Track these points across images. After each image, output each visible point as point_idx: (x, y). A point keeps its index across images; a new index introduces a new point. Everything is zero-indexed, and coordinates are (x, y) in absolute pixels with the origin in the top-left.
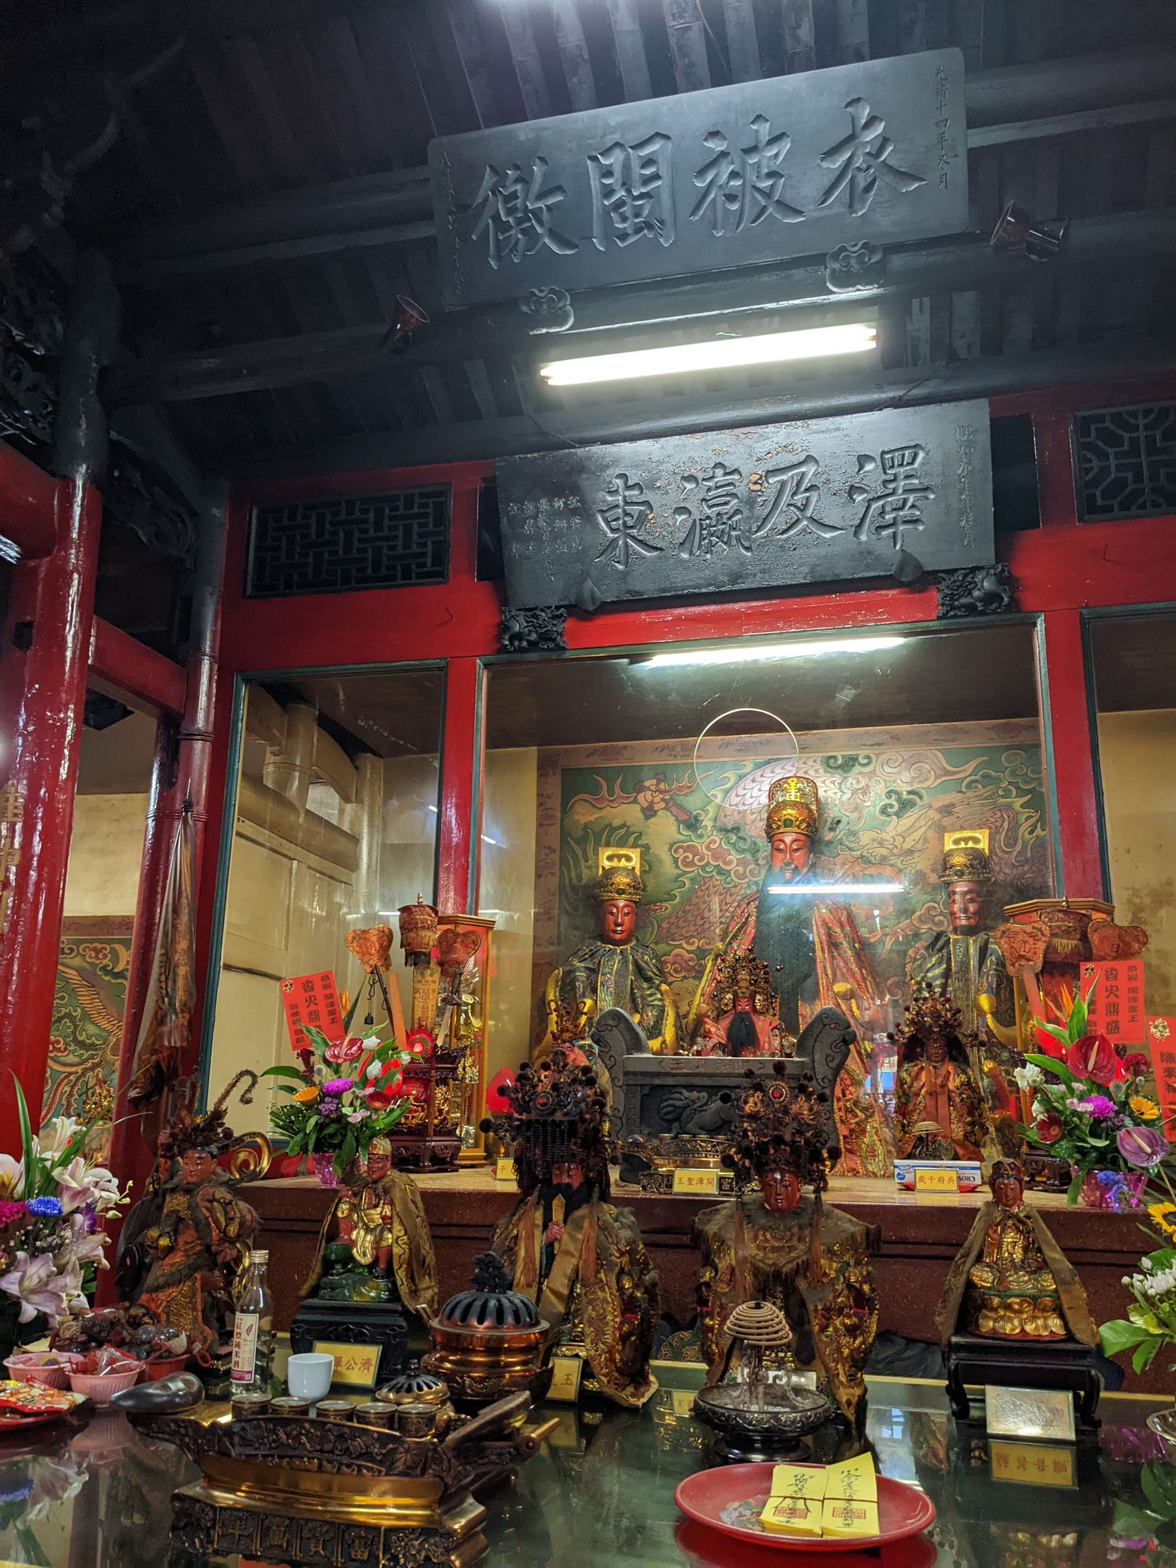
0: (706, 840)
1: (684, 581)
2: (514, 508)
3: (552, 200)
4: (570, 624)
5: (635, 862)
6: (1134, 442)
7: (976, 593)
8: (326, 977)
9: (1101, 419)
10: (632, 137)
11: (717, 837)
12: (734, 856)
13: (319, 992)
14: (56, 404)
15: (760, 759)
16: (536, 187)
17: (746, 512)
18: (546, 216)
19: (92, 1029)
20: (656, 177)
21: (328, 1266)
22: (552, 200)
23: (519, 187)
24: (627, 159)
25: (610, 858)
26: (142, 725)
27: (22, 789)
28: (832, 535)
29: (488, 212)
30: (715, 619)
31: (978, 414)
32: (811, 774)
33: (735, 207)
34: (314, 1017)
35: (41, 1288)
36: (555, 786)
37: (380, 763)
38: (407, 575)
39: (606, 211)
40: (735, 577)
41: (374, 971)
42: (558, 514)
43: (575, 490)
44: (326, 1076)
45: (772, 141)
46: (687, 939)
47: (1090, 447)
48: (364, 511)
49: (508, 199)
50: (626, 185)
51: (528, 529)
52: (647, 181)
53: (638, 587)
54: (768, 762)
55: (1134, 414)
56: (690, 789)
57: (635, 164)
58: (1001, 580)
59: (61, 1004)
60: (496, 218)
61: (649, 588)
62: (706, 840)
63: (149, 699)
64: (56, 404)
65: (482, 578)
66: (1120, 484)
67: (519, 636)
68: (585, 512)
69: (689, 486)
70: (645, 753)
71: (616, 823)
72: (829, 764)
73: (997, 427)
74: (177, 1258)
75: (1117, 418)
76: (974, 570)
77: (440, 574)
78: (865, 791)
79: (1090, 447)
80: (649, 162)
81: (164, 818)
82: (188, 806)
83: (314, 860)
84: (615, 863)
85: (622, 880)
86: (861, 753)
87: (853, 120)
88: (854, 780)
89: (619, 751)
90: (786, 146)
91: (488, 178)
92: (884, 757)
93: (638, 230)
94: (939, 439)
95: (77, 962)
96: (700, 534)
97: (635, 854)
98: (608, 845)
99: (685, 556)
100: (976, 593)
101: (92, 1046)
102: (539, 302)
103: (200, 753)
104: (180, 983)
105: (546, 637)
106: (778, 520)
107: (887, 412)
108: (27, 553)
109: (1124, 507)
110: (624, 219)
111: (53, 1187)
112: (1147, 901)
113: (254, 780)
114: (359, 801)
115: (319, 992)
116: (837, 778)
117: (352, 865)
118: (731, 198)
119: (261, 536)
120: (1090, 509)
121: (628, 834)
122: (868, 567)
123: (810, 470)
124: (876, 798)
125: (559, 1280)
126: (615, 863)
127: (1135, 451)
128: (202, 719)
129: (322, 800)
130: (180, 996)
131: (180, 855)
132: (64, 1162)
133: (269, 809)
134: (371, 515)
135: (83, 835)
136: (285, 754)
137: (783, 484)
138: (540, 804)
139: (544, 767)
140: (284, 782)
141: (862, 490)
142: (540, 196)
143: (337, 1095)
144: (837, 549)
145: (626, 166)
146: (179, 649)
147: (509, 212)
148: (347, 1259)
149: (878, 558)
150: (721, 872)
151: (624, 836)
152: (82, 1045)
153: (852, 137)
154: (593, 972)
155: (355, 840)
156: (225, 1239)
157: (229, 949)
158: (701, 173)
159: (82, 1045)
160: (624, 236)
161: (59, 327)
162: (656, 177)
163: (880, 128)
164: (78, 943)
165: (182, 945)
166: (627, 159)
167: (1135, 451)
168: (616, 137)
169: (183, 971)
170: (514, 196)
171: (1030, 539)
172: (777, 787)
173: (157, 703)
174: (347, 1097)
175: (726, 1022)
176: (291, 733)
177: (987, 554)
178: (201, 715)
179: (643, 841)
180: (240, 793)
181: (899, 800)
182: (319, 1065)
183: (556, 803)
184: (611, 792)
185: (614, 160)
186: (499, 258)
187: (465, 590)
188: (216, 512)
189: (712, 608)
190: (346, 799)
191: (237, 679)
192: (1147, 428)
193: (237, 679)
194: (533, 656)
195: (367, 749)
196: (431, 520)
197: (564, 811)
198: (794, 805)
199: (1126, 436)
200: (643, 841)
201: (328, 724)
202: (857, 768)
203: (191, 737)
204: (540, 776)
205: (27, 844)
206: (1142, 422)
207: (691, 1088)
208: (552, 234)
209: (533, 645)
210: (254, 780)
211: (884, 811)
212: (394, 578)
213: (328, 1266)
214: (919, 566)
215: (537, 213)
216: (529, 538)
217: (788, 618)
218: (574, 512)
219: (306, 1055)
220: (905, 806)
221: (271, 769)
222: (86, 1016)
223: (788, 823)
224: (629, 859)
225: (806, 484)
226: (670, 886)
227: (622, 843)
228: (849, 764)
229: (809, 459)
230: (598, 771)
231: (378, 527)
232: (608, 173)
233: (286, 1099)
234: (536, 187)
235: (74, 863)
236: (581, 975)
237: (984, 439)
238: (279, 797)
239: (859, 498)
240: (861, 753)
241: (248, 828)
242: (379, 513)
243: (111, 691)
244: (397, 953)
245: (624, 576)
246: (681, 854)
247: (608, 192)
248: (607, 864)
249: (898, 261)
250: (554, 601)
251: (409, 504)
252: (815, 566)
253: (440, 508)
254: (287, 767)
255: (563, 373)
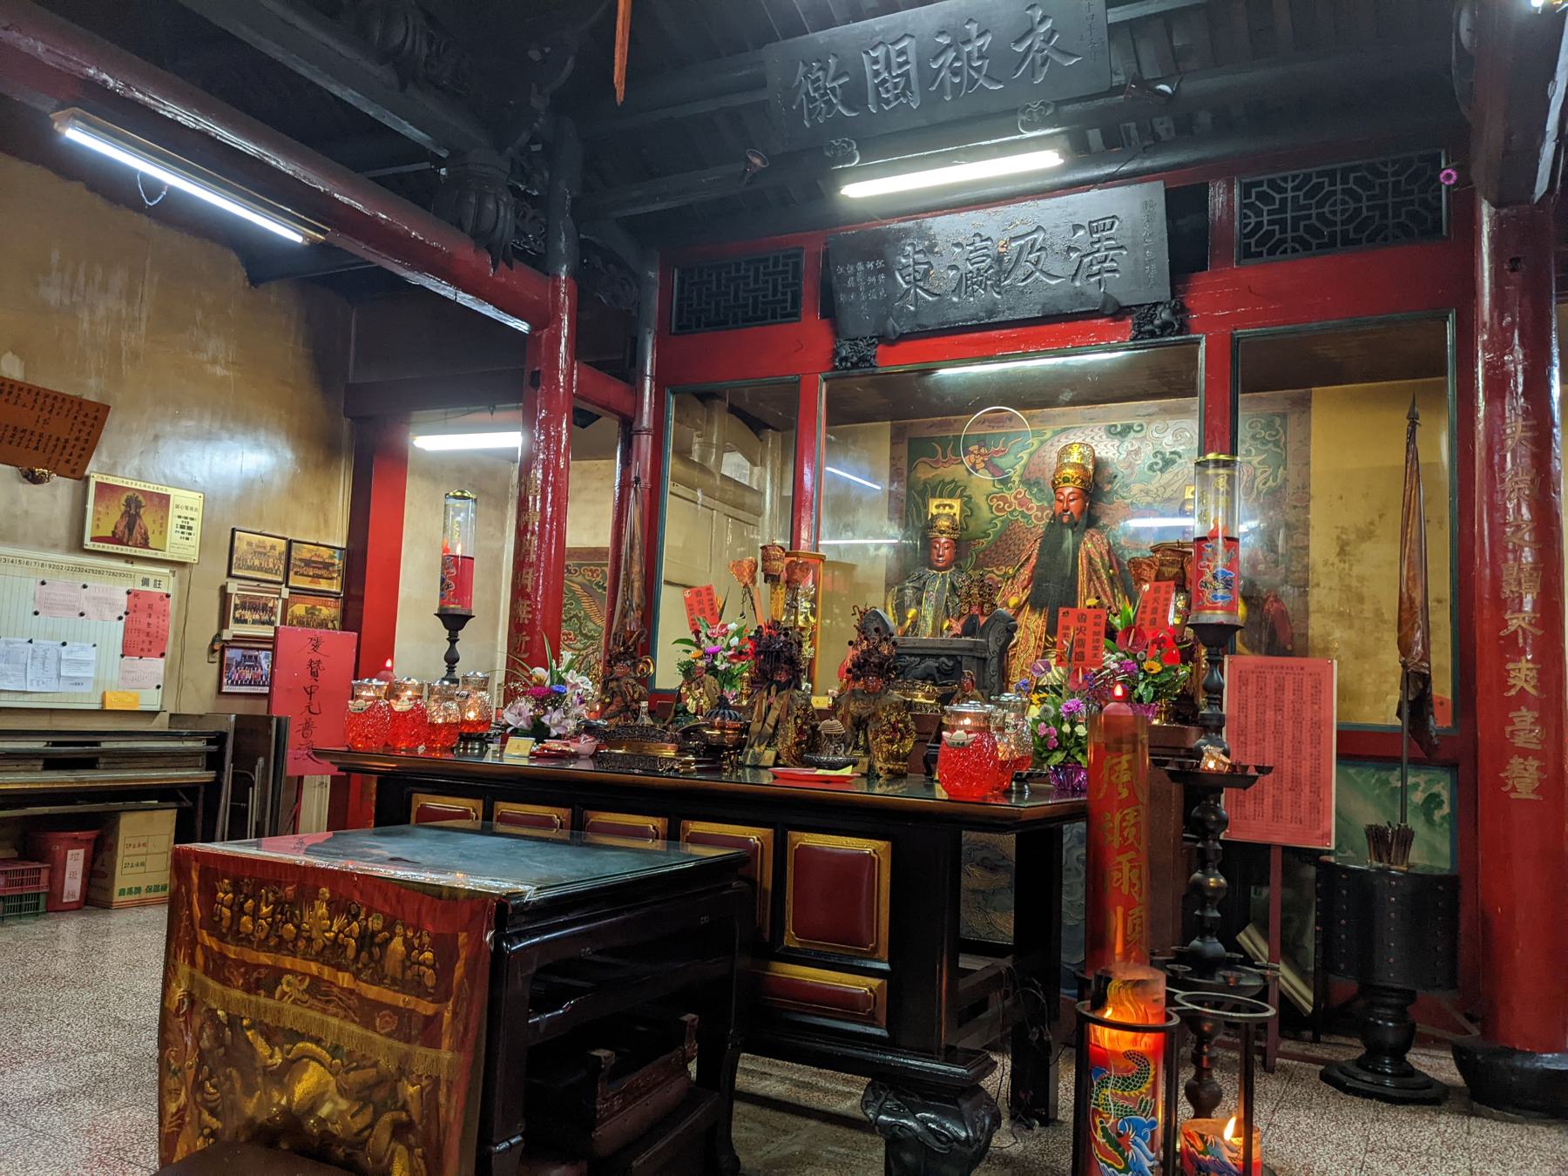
0: (1014, 492)
1: (954, 317)
2: (840, 270)
3: (841, 81)
4: (880, 348)
5: (957, 510)
6: (1283, 201)
7: (1157, 322)
8: (709, 589)
9: (1260, 184)
10: (892, 37)
11: (1022, 489)
12: (1035, 504)
13: (705, 597)
14: (547, 226)
15: (1058, 428)
16: (832, 71)
17: (996, 267)
18: (838, 91)
19: (591, 626)
20: (906, 62)
21: (677, 713)
22: (841, 81)
23: (820, 73)
24: (888, 52)
25: (938, 507)
26: (609, 426)
27: (539, 475)
28: (1053, 281)
29: (803, 90)
30: (978, 343)
31: (1154, 193)
32: (1088, 440)
33: (957, 80)
34: (702, 611)
35: (559, 724)
36: (903, 449)
37: (779, 436)
38: (774, 317)
39: (877, 86)
40: (991, 313)
41: (746, 586)
42: (868, 272)
43: (881, 256)
44: (707, 645)
45: (979, 36)
46: (997, 567)
47: (1250, 206)
48: (747, 270)
49: (813, 82)
50: (888, 67)
51: (850, 283)
52: (901, 65)
53: (924, 322)
54: (1064, 430)
55: (1285, 179)
56: (1004, 453)
57: (893, 55)
58: (1174, 312)
59: (570, 607)
60: (807, 94)
61: (931, 322)
62: (1014, 492)
63: (612, 411)
64: (547, 226)
65: (823, 317)
66: (1271, 233)
67: (845, 359)
68: (888, 271)
69: (957, 250)
70: (970, 425)
71: (948, 479)
72: (1111, 432)
73: (1170, 195)
74: (613, 707)
75: (1272, 184)
76: (1155, 305)
77: (795, 315)
78: (1137, 452)
79: (1250, 206)
80: (901, 53)
81: (625, 485)
82: (637, 480)
83: (728, 509)
84: (941, 510)
85: (944, 523)
86: (1136, 422)
87: (1032, 18)
88: (1130, 443)
89: (950, 424)
90: (989, 38)
91: (802, 69)
92: (1153, 426)
93: (897, 97)
94: (1128, 209)
95: (580, 579)
96: (964, 284)
97: (957, 504)
98: (933, 496)
99: (955, 299)
100: (1157, 322)
101: (592, 637)
102: (836, 149)
103: (645, 443)
104: (636, 592)
105: (863, 359)
106: (1019, 273)
107: (1094, 192)
108: (534, 328)
109: (1271, 252)
110: (888, 91)
111: (562, 681)
112: (1353, 537)
113: (683, 454)
114: (763, 464)
115: (705, 597)
116: (1116, 442)
117: (759, 513)
118: (955, 72)
119: (681, 290)
120: (1247, 253)
121: (934, 489)
122: (1082, 305)
123: (1040, 236)
124: (1146, 456)
125: (771, 720)
126: (941, 510)
127: (1282, 209)
128: (646, 421)
129: (734, 465)
130: (636, 600)
131: (634, 513)
132: (567, 671)
133: (696, 475)
134: (751, 274)
135: (580, 491)
136: (706, 436)
137: (1022, 247)
138: (892, 466)
139: (896, 438)
140: (704, 456)
141: (1076, 249)
142: (834, 80)
143: (715, 655)
144: (1061, 292)
145: (888, 58)
146: (628, 373)
147: (816, 90)
148: (685, 711)
149: (1089, 297)
150: (1024, 516)
151: (952, 489)
152: (586, 636)
153: (1032, 30)
154: (920, 590)
155: (761, 493)
156: (633, 700)
157: (667, 570)
158: (936, 58)
159: (586, 636)
160: (888, 102)
161: (547, 175)
162: (906, 62)
163: (1048, 24)
164: (580, 566)
165: (636, 569)
166: (888, 52)
167: (1282, 209)
168: (880, 38)
169: (636, 584)
170: (818, 79)
171: (1200, 280)
172: (1065, 451)
173: (618, 413)
174: (720, 657)
175: (963, 621)
176: (709, 421)
177: (1164, 293)
178: (645, 417)
179: (967, 493)
180: (672, 465)
181: (1163, 459)
182: (703, 638)
183: (904, 463)
184: (945, 456)
185: (879, 53)
186: (810, 120)
187: (812, 324)
188: (652, 274)
189: (977, 335)
190: (754, 464)
191: (667, 391)
192: (1293, 189)
193: (667, 391)
194: (856, 372)
195: (768, 427)
196: (790, 276)
197: (910, 471)
198: (1074, 465)
199: (1277, 196)
200: (967, 493)
201: (734, 410)
202: (1132, 434)
203: (639, 432)
204: (893, 444)
205: (543, 508)
206: (1290, 185)
207: (911, 655)
208: (844, 103)
209: (855, 366)
210: (683, 454)
211: (1151, 468)
212: (765, 318)
213: (677, 713)
214: (1117, 303)
215: (833, 90)
216: (851, 290)
217: (1027, 341)
218: (880, 271)
219: (697, 633)
220: (1168, 463)
221: (696, 447)
222: (587, 617)
223: (1066, 480)
224: (951, 507)
225: (1038, 246)
226: (985, 527)
227: (951, 496)
228: (1127, 429)
229: (1039, 228)
230: (932, 439)
231: (756, 281)
232: (875, 61)
233: (687, 658)
234: (832, 71)
235: (572, 510)
236: (909, 592)
237: (1160, 209)
238: (702, 468)
239: (1074, 255)
240: (1136, 422)
241: (681, 490)
242: (757, 270)
243: (588, 407)
244: (760, 575)
245: (915, 314)
246: (995, 503)
247: (877, 74)
248: (934, 511)
249: (1068, 108)
250: (869, 333)
251: (776, 265)
252: (1044, 305)
253: (797, 266)
254: (707, 445)
255: (862, 190)
